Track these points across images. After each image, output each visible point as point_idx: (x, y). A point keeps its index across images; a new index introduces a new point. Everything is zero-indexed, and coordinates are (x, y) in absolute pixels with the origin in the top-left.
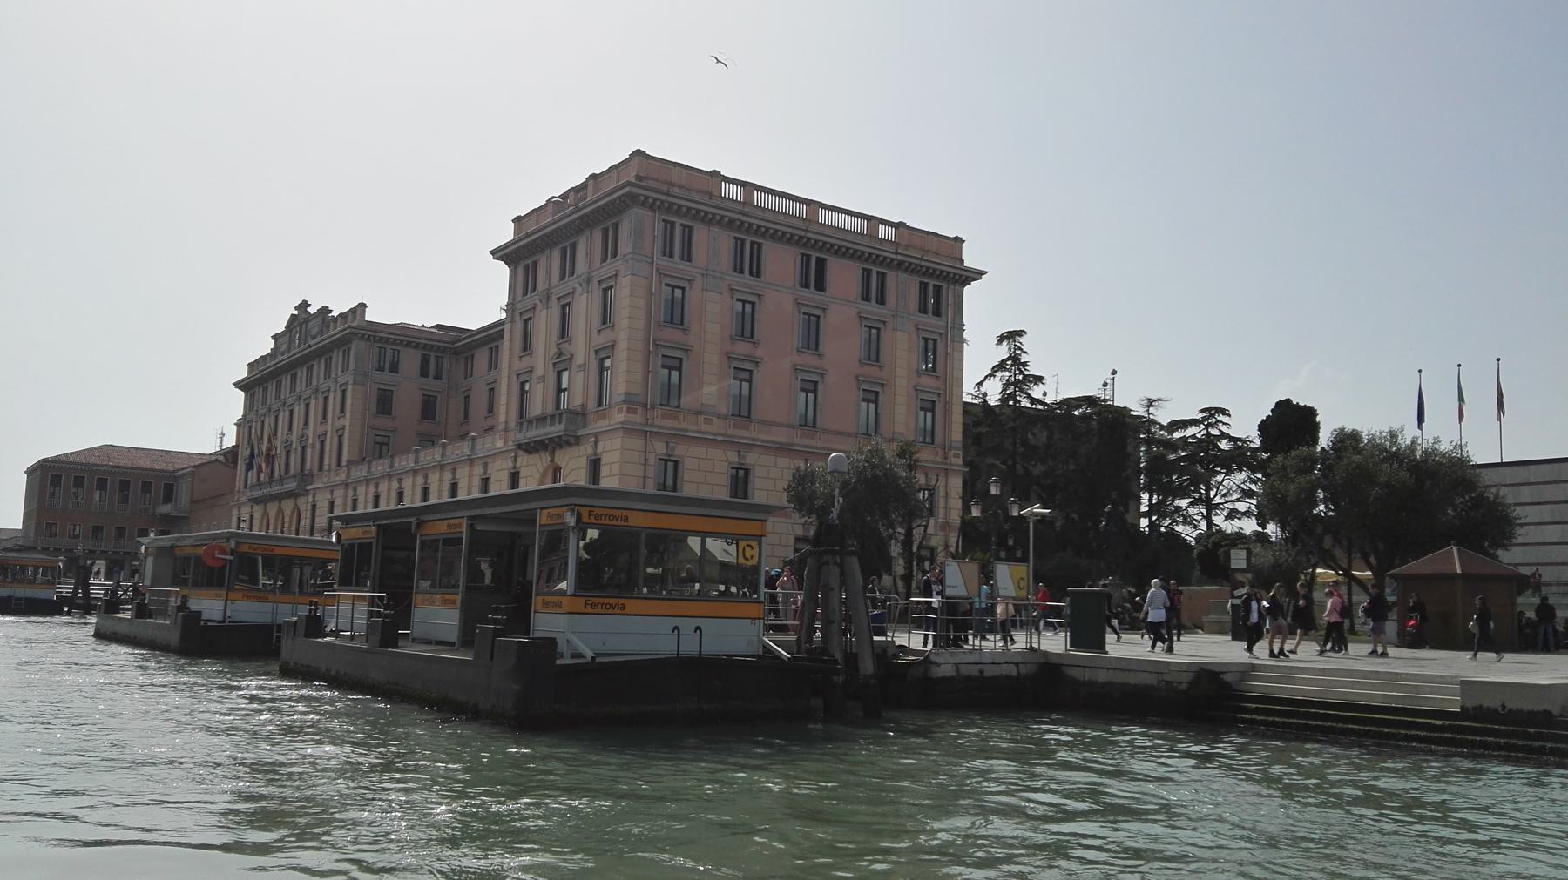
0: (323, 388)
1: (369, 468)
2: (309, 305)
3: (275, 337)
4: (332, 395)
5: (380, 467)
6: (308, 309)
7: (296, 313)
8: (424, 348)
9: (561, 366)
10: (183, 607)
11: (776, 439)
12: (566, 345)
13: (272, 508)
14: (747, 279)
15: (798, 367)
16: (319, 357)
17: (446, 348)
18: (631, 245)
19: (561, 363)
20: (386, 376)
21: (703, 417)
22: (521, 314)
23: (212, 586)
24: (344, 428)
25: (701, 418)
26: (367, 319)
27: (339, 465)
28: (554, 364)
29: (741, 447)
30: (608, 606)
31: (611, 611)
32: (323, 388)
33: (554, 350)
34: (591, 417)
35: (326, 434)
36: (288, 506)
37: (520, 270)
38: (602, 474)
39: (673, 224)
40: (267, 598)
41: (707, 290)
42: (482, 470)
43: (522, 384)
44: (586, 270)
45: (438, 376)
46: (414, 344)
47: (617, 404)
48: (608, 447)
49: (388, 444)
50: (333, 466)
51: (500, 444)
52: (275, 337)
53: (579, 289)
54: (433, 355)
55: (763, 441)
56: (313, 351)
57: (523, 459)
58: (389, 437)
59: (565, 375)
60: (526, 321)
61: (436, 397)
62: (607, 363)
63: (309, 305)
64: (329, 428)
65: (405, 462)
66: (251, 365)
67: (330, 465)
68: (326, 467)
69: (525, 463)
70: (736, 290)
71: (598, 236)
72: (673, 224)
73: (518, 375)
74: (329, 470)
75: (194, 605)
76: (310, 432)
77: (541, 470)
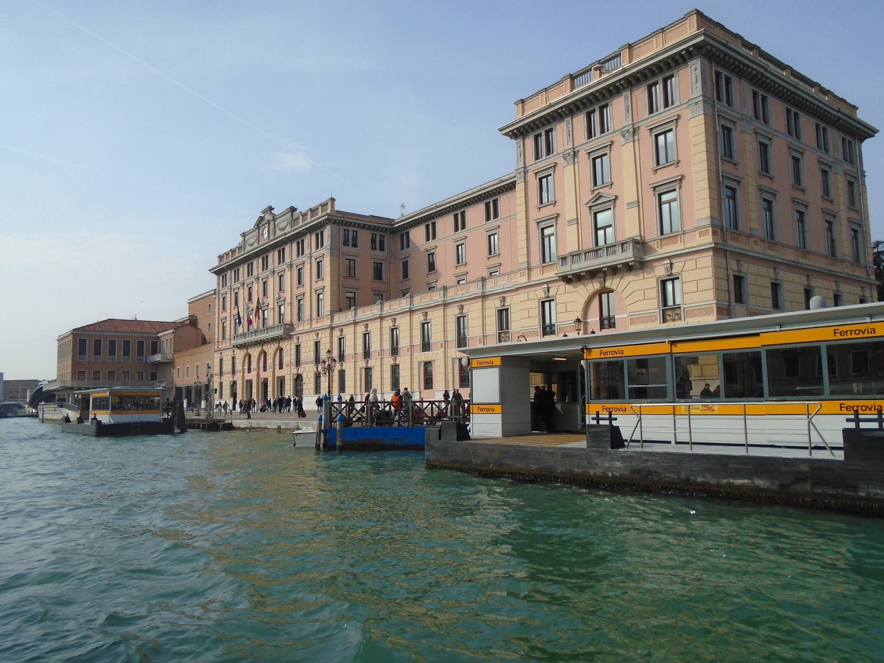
0: (247, 282)
1: (355, 314)
2: (273, 209)
3: (244, 235)
4: (228, 296)
5: (348, 316)
6: (273, 212)
7: (262, 215)
8: (373, 229)
9: (280, 304)
10: (95, 419)
11: (788, 258)
12: (282, 294)
13: (255, 352)
14: (761, 124)
15: (796, 200)
16: (578, 109)
17: (387, 229)
18: (329, 242)
19: (280, 302)
20: (350, 249)
21: (753, 239)
22: (316, 259)
23: (756, 393)
24: (226, 318)
25: (752, 240)
26: (335, 209)
27: (224, 337)
28: (278, 303)
29: (776, 265)
30: (616, 410)
31: (489, 412)
32: (247, 282)
33: (277, 296)
34: (296, 326)
35: (226, 319)
36: (270, 349)
37: (221, 277)
38: (236, 362)
39: (348, 230)
40: (493, 410)
41: (744, 132)
42: (364, 329)
43: (299, 301)
44: (273, 267)
45: (382, 249)
46: (367, 226)
47: (326, 316)
48: (323, 336)
49: (354, 298)
50: (220, 339)
51: (228, 344)
52: (244, 235)
53: (287, 269)
54: (378, 234)
55: (788, 260)
56: (287, 238)
57: (237, 351)
58: (355, 293)
59: (282, 307)
60: (280, 276)
61: (382, 264)
62: (321, 296)
63: (273, 209)
64: (228, 315)
65: (365, 313)
66: (221, 258)
67: (218, 339)
68: (227, 337)
69: (323, 336)
70: (760, 134)
71: (260, 260)
72: (348, 230)
73: (316, 291)
74: (218, 342)
75: (99, 418)
76: (287, 295)
77: (274, 350)
